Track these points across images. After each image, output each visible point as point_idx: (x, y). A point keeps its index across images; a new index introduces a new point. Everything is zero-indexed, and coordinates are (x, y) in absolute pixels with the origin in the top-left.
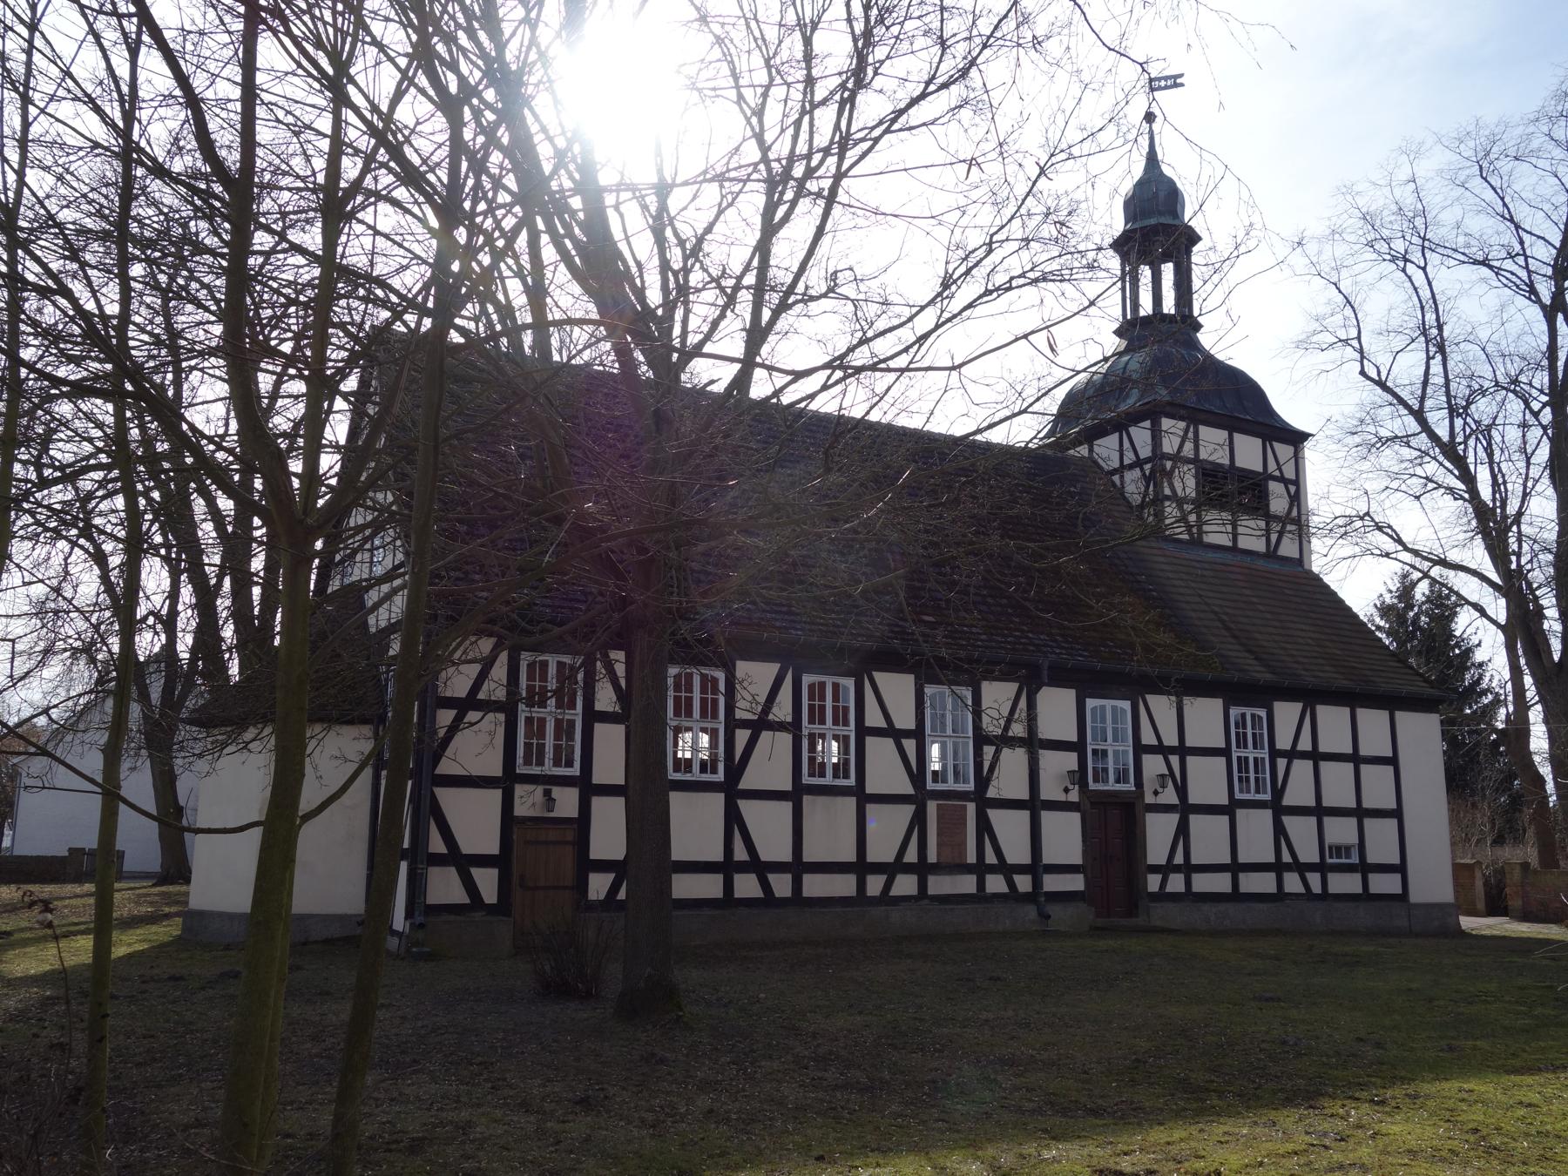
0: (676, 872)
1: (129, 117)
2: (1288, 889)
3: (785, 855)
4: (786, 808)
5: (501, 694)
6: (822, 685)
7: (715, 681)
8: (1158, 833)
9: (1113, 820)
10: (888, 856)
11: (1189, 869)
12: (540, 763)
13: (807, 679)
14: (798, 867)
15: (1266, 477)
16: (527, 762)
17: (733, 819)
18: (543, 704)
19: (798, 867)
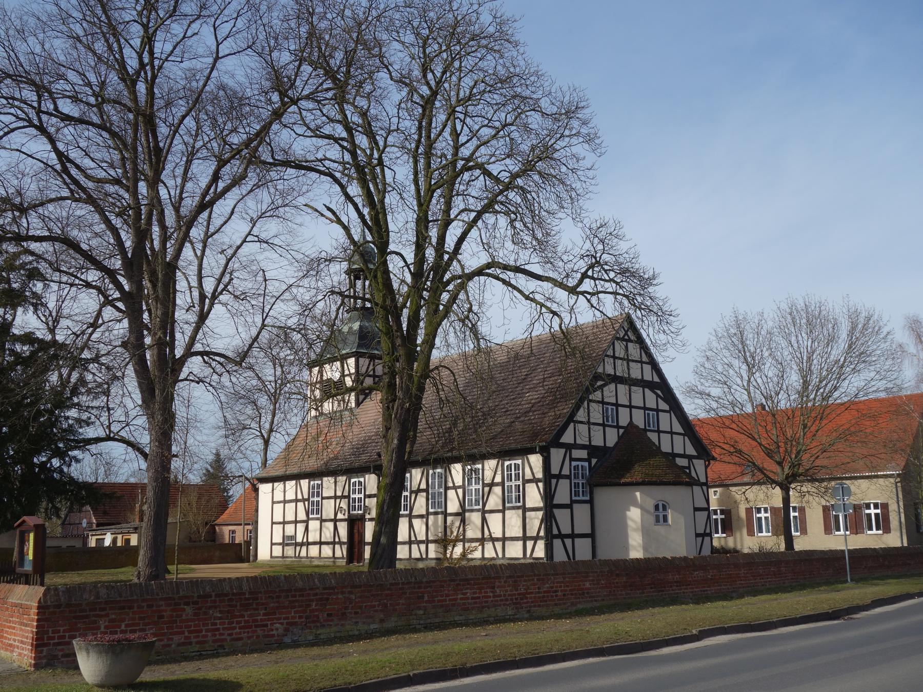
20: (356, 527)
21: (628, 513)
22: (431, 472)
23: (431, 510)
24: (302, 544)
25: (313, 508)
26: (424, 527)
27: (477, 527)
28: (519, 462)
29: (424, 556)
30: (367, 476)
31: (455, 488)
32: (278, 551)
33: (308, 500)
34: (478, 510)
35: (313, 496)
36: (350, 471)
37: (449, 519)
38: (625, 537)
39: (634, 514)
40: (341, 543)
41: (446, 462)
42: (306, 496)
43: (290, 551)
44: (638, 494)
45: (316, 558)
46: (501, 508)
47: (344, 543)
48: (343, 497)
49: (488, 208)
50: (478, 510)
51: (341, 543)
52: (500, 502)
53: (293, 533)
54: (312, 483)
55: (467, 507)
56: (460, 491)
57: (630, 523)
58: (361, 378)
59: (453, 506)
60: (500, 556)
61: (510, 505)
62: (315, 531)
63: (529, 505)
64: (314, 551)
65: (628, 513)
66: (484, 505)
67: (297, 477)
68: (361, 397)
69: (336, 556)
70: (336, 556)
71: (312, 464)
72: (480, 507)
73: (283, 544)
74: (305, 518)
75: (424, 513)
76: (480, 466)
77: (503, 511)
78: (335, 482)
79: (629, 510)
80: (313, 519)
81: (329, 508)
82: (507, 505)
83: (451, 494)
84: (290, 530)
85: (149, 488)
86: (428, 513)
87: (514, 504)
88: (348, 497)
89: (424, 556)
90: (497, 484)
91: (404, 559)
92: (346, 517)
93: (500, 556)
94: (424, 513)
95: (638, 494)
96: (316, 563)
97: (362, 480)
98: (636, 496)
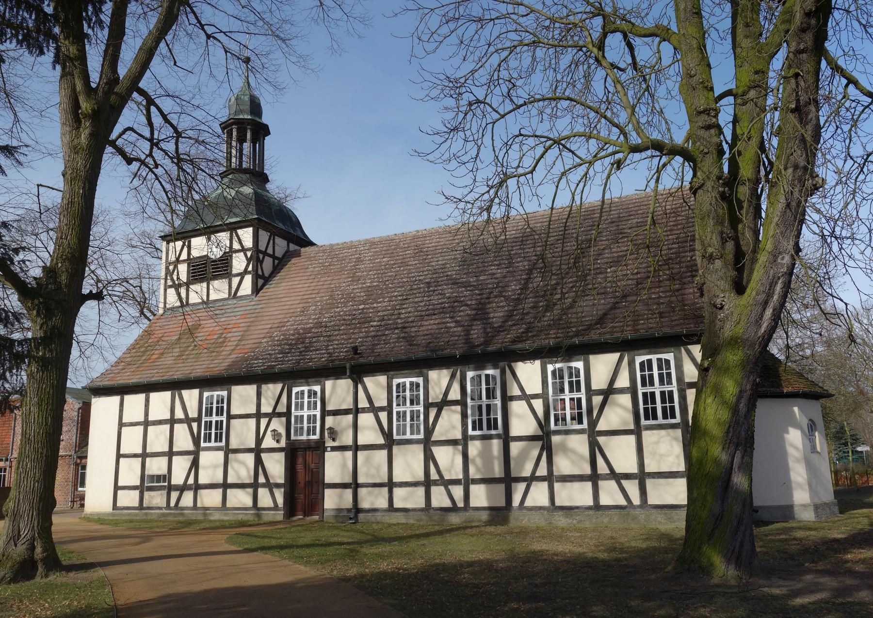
0: (473, 483)
1: (550, 139)
2: (604, 500)
3: (634, 469)
4: (632, 439)
5: (458, 397)
6: (650, 362)
7: (668, 362)
8: (335, 467)
9: (304, 459)
10: (181, 482)
11: (197, 487)
12: (404, 433)
13: (639, 359)
14: (642, 477)
15: (189, 260)
16: (398, 434)
17: (429, 457)
18: (309, 417)
19: (642, 477)
20: (300, 460)
21: (786, 436)
22: (470, 374)
23: (471, 432)
24: (182, 489)
25: (211, 430)
26: (459, 459)
27: (582, 457)
28: (670, 356)
29: (461, 504)
30: (329, 384)
31: (527, 398)
32: (129, 499)
33: (198, 420)
34: (418, 442)
35: (209, 412)
36: (290, 376)
37: (515, 448)
38: (786, 469)
39: (794, 437)
40: (270, 486)
41: (507, 357)
42: (193, 413)
43: (156, 499)
44: (796, 409)
45: (216, 509)
46: (632, 427)
47: (278, 486)
48: (274, 414)
49: (553, 46)
50: (418, 442)
51: (270, 486)
52: (630, 418)
53: (164, 471)
54: (206, 394)
55: (395, 437)
56: (538, 404)
57: (791, 451)
58: (261, 256)
59: (522, 422)
60: (636, 501)
61: (207, 445)
62: (216, 467)
63: (234, 444)
64: (211, 499)
65: (786, 436)
66: (593, 423)
67: (175, 386)
68: (260, 282)
69: (261, 504)
70: (261, 504)
71: (218, 365)
72: (223, 444)
73: (142, 488)
74: (190, 447)
75: (459, 436)
76: (579, 365)
77: (637, 432)
78: (259, 395)
79: (788, 433)
80: (473, 438)
81: (243, 433)
82: (643, 422)
83: (518, 408)
84: (156, 466)
85: (31, 392)
86: (466, 438)
87: (213, 444)
88: (288, 414)
89: (461, 504)
90: (622, 391)
91: (414, 510)
92: (283, 444)
93: (636, 501)
94: (459, 436)
95: (796, 409)
96: (216, 516)
97: (317, 388)
98: (794, 412)
